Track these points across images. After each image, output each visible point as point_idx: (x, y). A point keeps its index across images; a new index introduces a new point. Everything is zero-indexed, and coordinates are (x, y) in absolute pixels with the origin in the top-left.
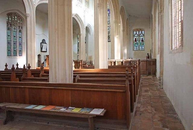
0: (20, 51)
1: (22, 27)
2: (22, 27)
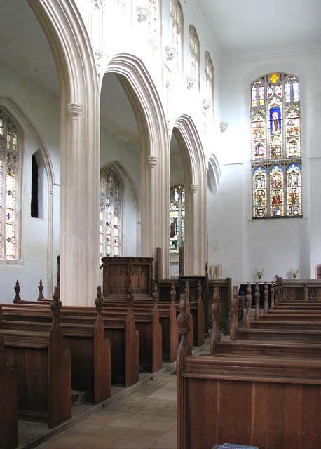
0: (259, 146)
1: (15, 157)
2: (15, 157)
